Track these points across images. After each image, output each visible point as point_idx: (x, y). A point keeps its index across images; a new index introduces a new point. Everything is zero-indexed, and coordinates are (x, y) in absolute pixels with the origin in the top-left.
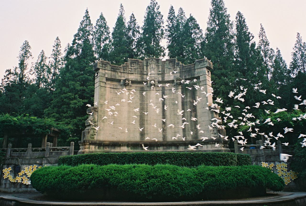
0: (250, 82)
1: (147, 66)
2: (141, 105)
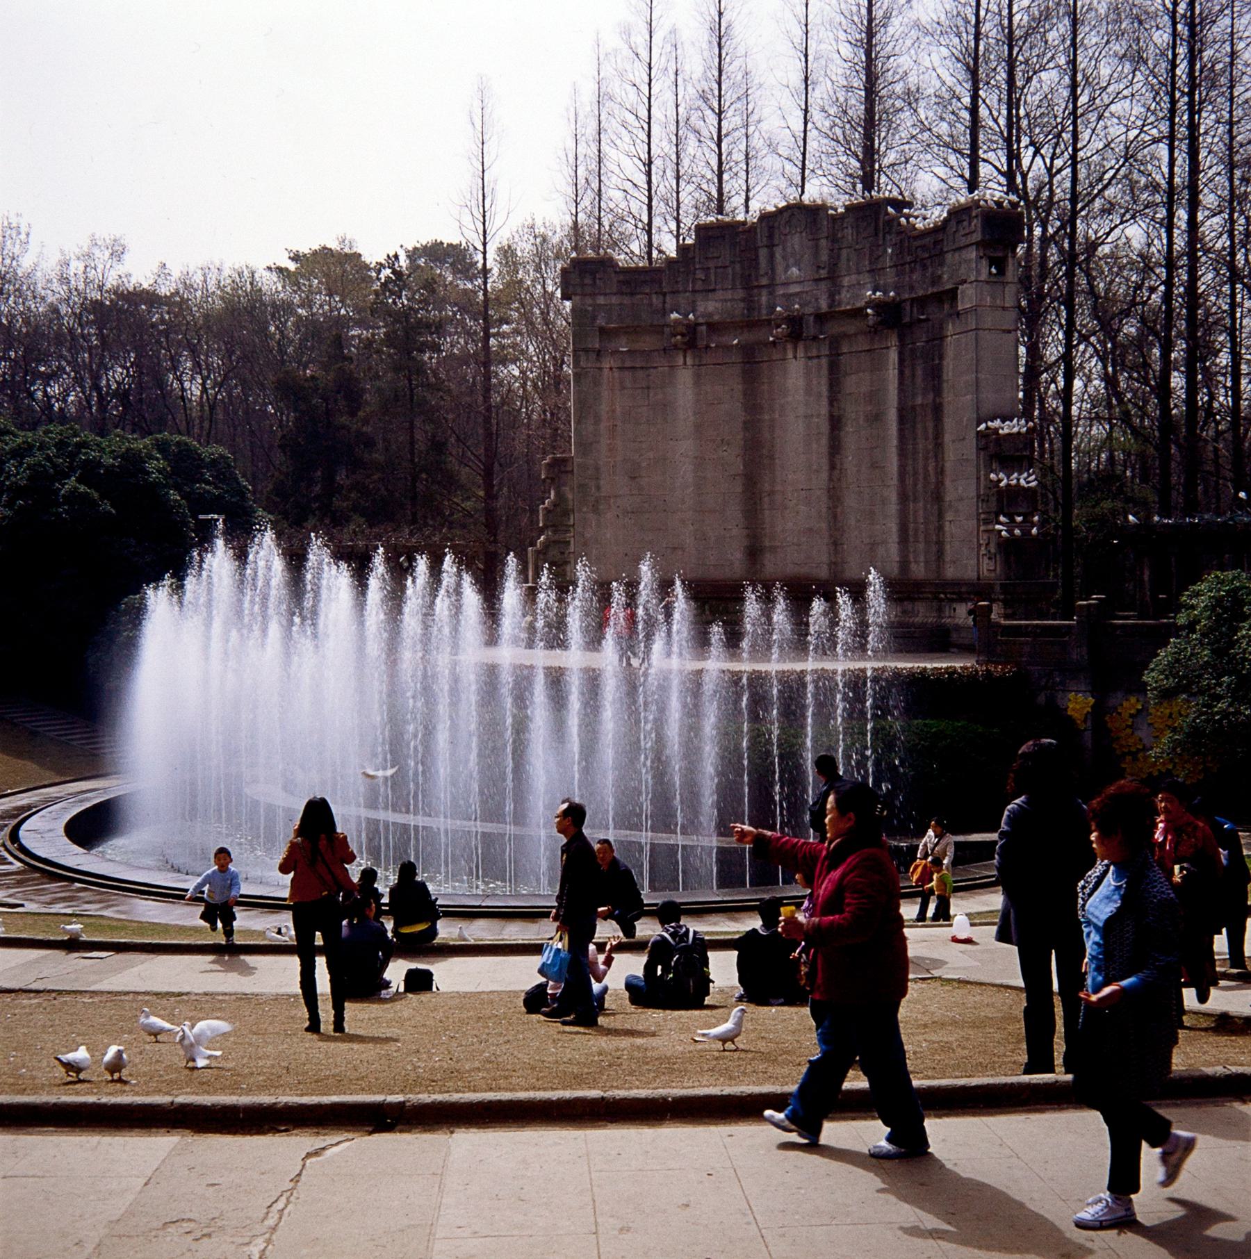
0: (1131, 518)
1: (771, 246)
2: (746, 429)
